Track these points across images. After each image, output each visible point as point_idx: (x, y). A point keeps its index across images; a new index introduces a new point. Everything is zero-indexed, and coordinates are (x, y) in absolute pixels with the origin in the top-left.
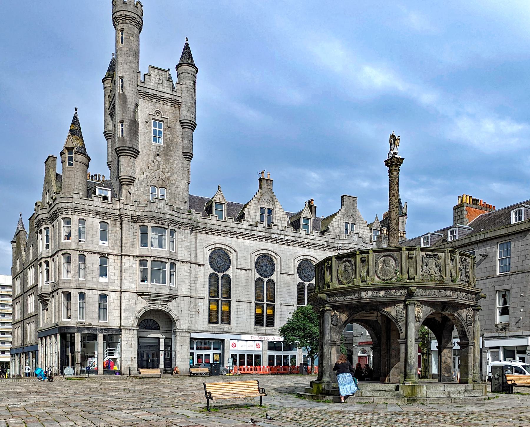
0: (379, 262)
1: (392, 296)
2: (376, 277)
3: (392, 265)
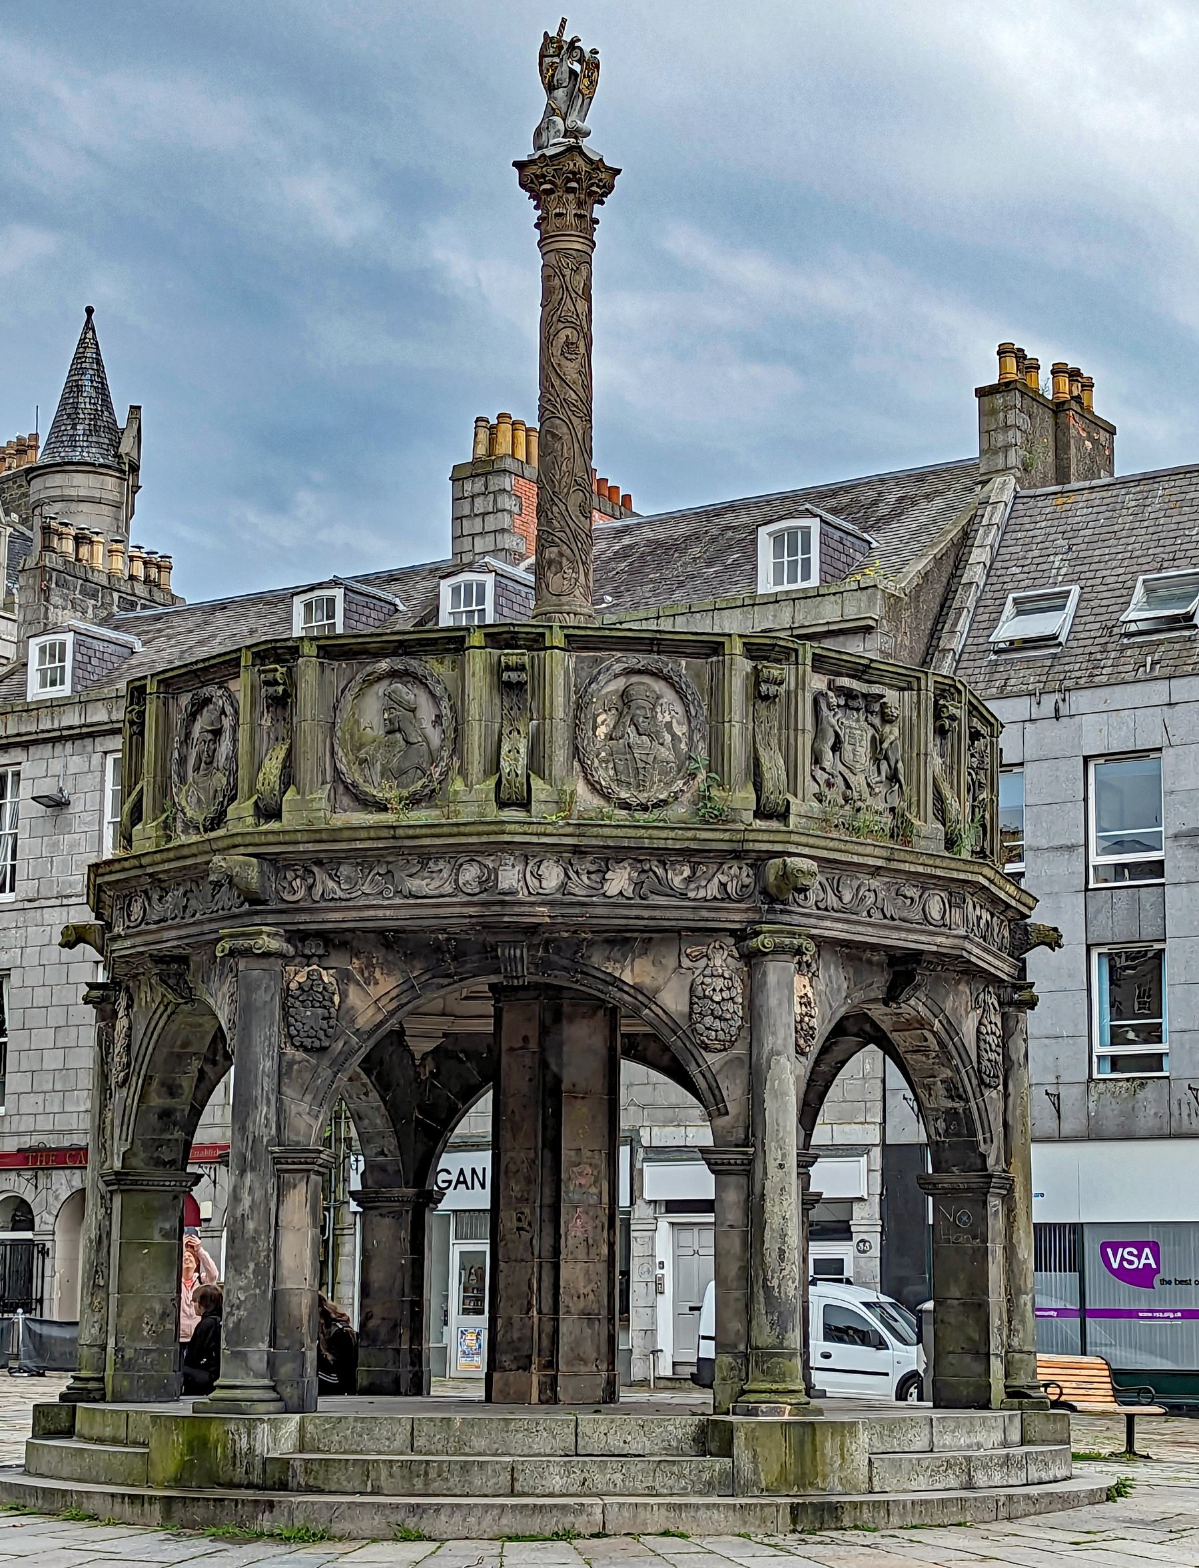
0: (597, 706)
1: (675, 902)
2: (581, 788)
3: (669, 726)
